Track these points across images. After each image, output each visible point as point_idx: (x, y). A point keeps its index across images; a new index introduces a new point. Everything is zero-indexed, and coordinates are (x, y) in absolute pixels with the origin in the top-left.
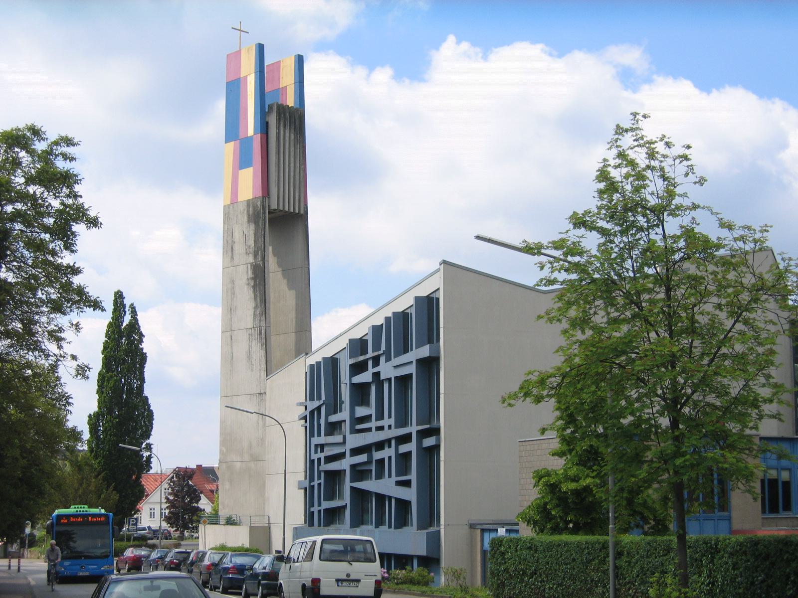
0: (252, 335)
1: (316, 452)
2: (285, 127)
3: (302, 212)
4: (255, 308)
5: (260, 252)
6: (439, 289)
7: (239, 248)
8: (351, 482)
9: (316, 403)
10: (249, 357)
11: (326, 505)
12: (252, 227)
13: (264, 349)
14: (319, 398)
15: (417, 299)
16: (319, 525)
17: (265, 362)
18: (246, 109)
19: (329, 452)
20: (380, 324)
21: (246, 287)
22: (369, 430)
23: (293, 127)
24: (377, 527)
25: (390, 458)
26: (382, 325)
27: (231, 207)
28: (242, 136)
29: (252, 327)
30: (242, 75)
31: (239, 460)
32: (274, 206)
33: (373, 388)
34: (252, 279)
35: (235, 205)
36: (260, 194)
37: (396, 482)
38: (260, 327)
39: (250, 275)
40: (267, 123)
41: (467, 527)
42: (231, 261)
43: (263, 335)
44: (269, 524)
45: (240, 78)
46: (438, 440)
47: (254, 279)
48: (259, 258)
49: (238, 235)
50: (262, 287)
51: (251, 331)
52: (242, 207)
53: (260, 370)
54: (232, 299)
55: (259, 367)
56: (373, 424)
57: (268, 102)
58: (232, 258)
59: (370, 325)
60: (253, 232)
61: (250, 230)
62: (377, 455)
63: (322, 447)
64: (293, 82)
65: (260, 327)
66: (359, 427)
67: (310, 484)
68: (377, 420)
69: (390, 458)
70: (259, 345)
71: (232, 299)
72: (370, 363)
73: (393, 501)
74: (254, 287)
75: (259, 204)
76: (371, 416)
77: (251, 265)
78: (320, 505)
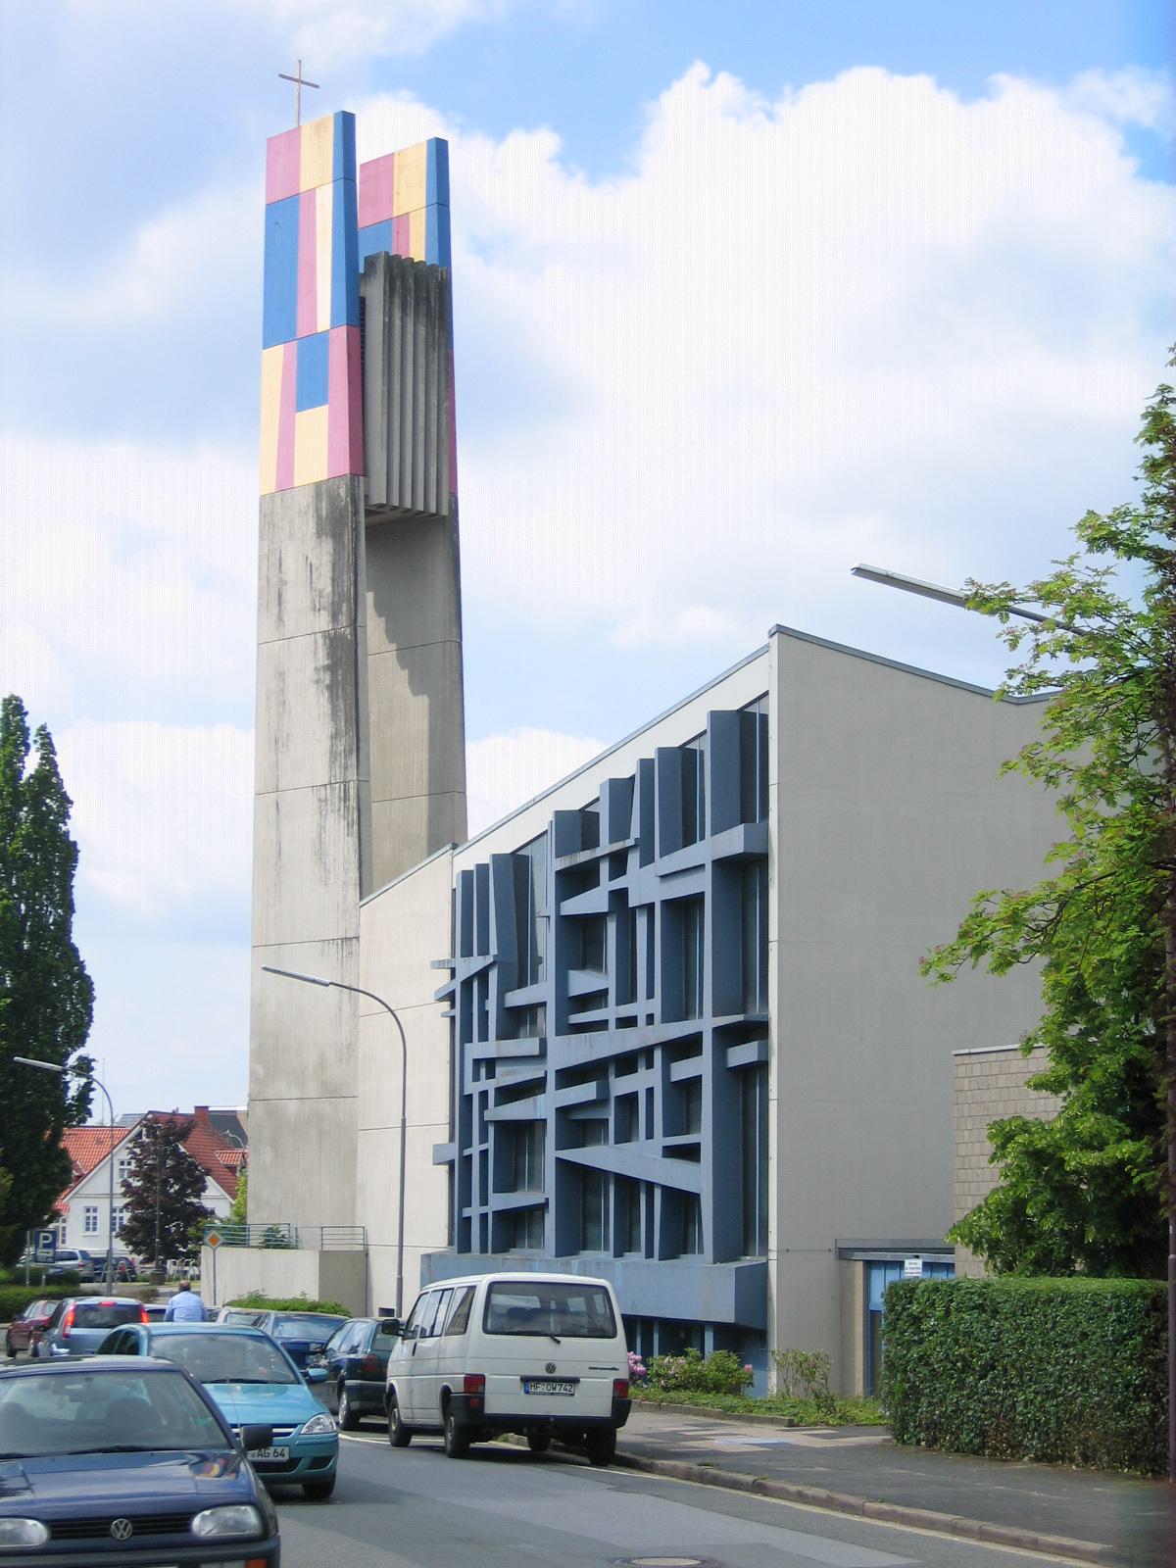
0: (326, 800)
1: (476, 1078)
4: (334, 737)
6: (766, 694)
7: (297, 597)
8: (559, 1146)
9: (477, 963)
11: (499, 1201)
12: (328, 546)
13: (356, 835)
14: (484, 951)
15: (716, 717)
16: (484, 1250)
17: (357, 865)
18: (313, 268)
19: (506, 1076)
20: (627, 776)
21: (312, 689)
22: (602, 1025)
23: (423, 309)
25: (650, 1091)
26: (632, 778)
27: (278, 500)
28: (302, 331)
30: (304, 187)
32: (379, 497)
33: (612, 928)
34: (327, 668)
36: (345, 468)
39: (323, 659)
40: (363, 301)
41: (832, 1256)
42: (278, 628)
43: (353, 803)
46: (765, 1050)
47: (332, 668)
48: (344, 620)
49: (293, 567)
50: (350, 689)
52: (304, 501)
56: (611, 1012)
57: (365, 250)
58: (280, 619)
61: (322, 554)
62: (621, 1086)
64: (424, 205)
65: (345, 783)
69: (650, 1091)
70: (343, 824)
72: (604, 868)
73: (658, 1193)
74: (332, 688)
75: (342, 492)
77: (324, 637)
78: (484, 1202)
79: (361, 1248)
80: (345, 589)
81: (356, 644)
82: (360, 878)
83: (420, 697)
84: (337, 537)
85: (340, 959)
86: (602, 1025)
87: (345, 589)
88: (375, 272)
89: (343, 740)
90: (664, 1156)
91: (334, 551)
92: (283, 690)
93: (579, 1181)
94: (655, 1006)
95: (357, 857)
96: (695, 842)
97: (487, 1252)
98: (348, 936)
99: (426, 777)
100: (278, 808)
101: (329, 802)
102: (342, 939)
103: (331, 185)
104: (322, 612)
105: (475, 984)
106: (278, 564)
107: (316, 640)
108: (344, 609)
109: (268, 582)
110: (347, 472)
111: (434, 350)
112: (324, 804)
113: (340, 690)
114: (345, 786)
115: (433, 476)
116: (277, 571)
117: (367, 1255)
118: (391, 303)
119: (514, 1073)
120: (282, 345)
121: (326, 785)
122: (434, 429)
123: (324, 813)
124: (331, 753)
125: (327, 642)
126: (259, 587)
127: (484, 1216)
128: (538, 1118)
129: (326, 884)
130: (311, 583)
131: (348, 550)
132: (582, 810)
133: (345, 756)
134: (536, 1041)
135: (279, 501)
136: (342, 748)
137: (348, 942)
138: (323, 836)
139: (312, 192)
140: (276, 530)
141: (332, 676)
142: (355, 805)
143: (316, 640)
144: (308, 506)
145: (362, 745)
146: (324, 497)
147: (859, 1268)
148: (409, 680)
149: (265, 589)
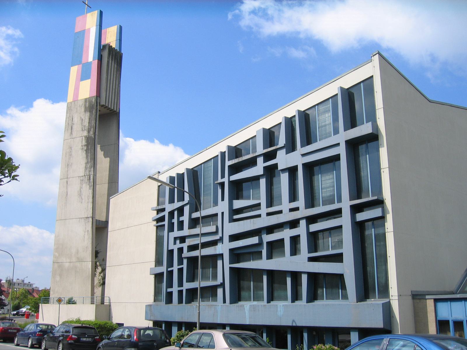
0: (83, 180)
1: (175, 243)
2: (112, 60)
3: (118, 111)
4: (87, 163)
5: (92, 130)
7: (77, 127)
9: (177, 204)
10: (80, 194)
11: (187, 285)
12: (88, 114)
13: (92, 189)
14: (181, 198)
15: (229, 147)
16: (180, 301)
17: (92, 197)
18: (88, 47)
19: (189, 242)
20: (181, 172)
21: (80, 151)
22: (259, 216)
23: (116, 61)
24: (268, 302)
26: (225, 152)
27: (73, 103)
28: (84, 61)
29: (83, 175)
30: (87, 27)
31: (68, 261)
32: (103, 103)
34: (86, 145)
35: (76, 102)
36: (95, 94)
37: (309, 258)
38: (90, 176)
39: (84, 143)
40: (102, 55)
41: (410, 298)
42: (70, 135)
43: (92, 180)
44: (110, 303)
45: (85, 30)
46: (384, 211)
47: (87, 145)
48: (92, 133)
49: (76, 120)
50: (93, 151)
51: (82, 177)
52: (81, 103)
53: (88, 202)
54: (69, 159)
55: (87, 201)
57: (103, 43)
58: (71, 133)
59: (169, 176)
60: (88, 117)
61: (86, 117)
63: (183, 239)
64: (115, 40)
65: (90, 176)
66: (236, 217)
67: (167, 269)
68: (268, 207)
70: (88, 186)
71: (69, 159)
73: (304, 278)
74: (87, 151)
75: (93, 100)
76: (259, 205)
77: (85, 137)
78: (180, 284)
79: (108, 304)
80: (93, 125)
81: (95, 139)
82: (93, 201)
83: (107, 158)
84: (91, 112)
85: (85, 223)
86: (259, 216)
87: (93, 125)
88: (105, 49)
89: (89, 164)
90: (308, 261)
91: (90, 115)
92: (71, 152)
93: (238, 276)
94: (301, 202)
95: (92, 195)
96: (317, 141)
97: (182, 303)
98: (88, 217)
99: (107, 178)
100: (67, 183)
101: (84, 181)
102: (86, 218)
103: (95, 27)
104: (85, 131)
105: (176, 213)
106: (72, 119)
107: (82, 138)
108: (92, 130)
109: (68, 124)
110: (95, 95)
111: (118, 71)
112: (82, 181)
113: (89, 151)
114: (89, 176)
115: (116, 102)
116: (71, 121)
117: (110, 306)
118: (109, 55)
119: (194, 240)
120: (77, 66)
121: (83, 176)
122: (117, 90)
123: (82, 184)
124: (85, 167)
125: (86, 138)
126: (65, 125)
127: (180, 292)
128: (218, 253)
129: (82, 202)
130: (82, 124)
131: (94, 114)
132: (192, 169)
133: (90, 168)
134: (215, 227)
135: (73, 104)
136: (89, 166)
137: (88, 218)
138: (81, 189)
139: (89, 29)
140: (72, 111)
141: (87, 147)
142: (92, 181)
143: (82, 138)
144: (82, 104)
145: (95, 165)
146: (88, 102)
147: (430, 304)
148: (104, 154)
149: (67, 126)
